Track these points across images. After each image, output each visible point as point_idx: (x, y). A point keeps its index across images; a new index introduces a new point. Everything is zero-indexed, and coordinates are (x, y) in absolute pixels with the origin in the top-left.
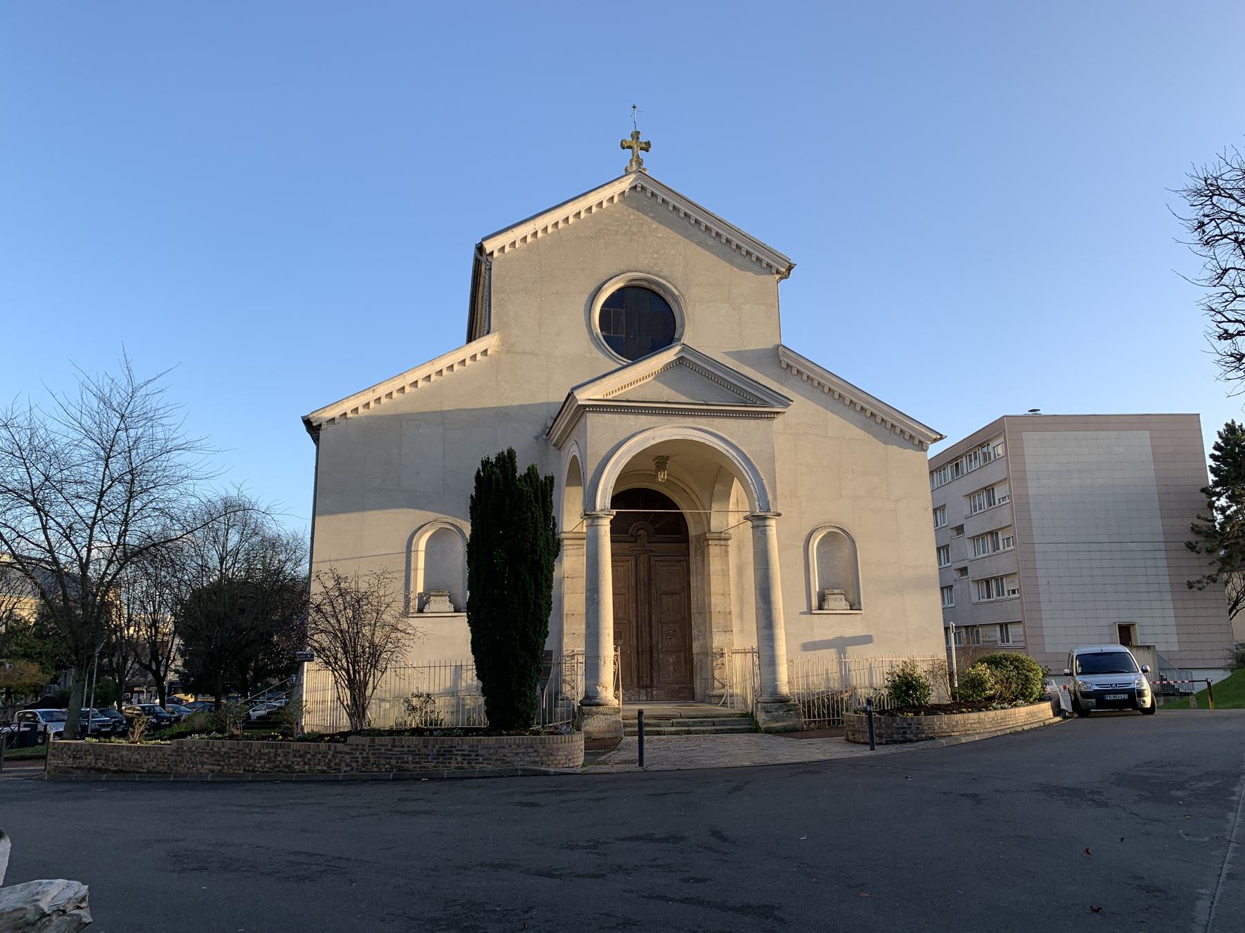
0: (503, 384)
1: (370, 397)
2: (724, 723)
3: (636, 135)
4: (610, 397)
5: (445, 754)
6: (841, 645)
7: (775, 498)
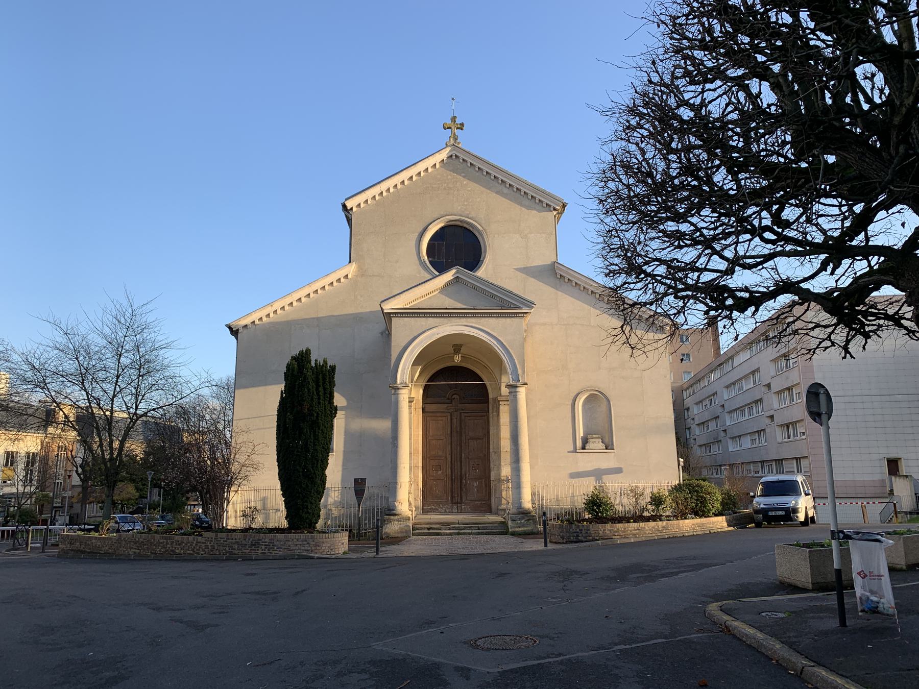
0: (359, 297)
1: (270, 310)
2: (483, 528)
3: (454, 119)
4: (408, 306)
5: (255, 544)
6: (598, 474)
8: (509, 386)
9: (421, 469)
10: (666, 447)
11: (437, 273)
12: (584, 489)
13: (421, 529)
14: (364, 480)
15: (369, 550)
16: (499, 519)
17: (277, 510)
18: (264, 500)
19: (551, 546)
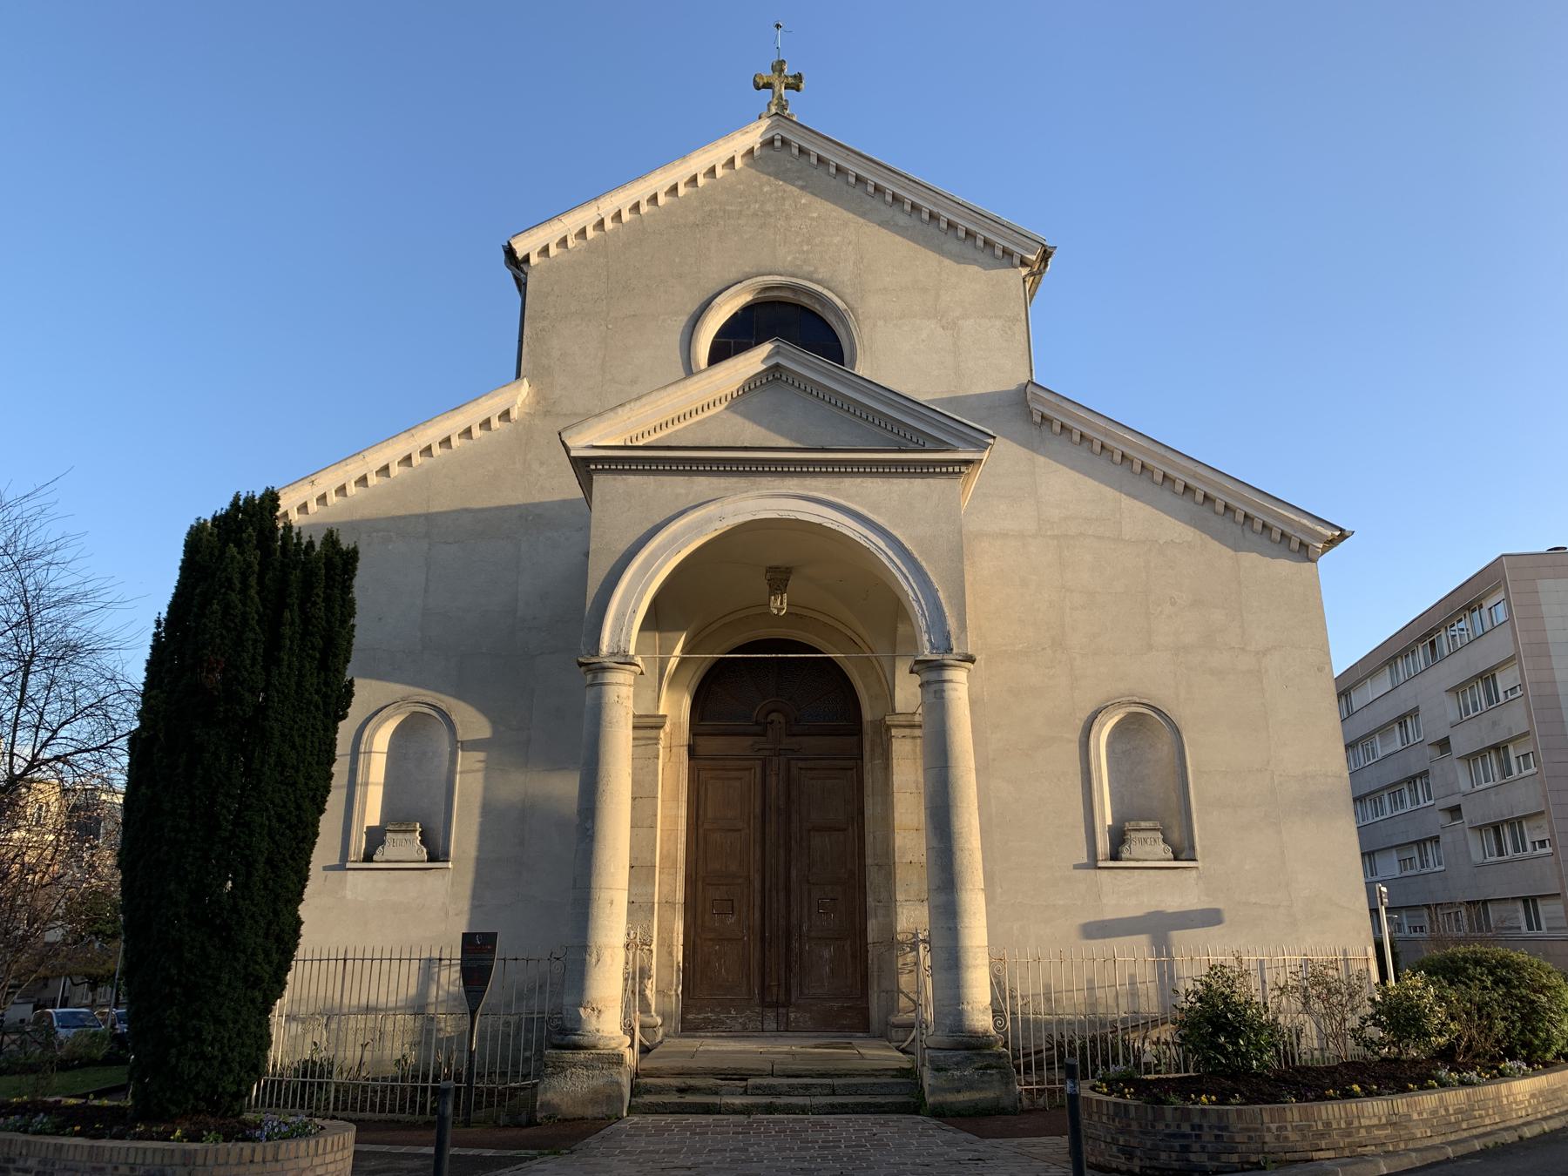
3: (778, 67)
4: (641, 443)
6: (1159, 928)
9: (680, 909)
13: (660, 1090)
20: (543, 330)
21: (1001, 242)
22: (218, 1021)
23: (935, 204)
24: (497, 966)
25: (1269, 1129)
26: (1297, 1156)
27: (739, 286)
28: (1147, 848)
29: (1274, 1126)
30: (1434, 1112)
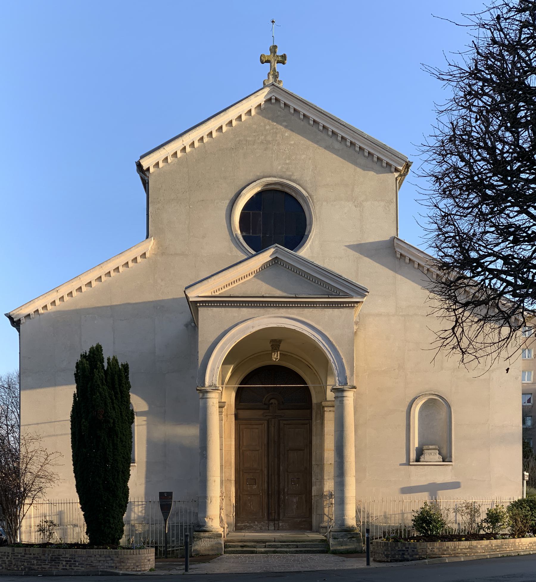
1: (54, 296)
2: (303, 546)
3: (273, 49)
4: (217, 294)
5: (55, 560)
6: (433, 489)
7: (352, 374)
8: (334, 390)
9: (233, 483)
10: (510, 458)
11: (253, 252)
12: (417, 503)
13: (234, 546)
14: (170, 494)
15: (178, 568)
16: (320, 537)
17: (75, 526)
18: (60, 514)
19: (373, 565)
20: (158, 209)
21: (385, 159)
22: (114, 518)
23: (353, 137)
24: (173, 503)
25: (429, 549)
26: (437, 556)
27: (254, 184)
28: (431, 457)
29: (430, 548)
30: (487, 546)
